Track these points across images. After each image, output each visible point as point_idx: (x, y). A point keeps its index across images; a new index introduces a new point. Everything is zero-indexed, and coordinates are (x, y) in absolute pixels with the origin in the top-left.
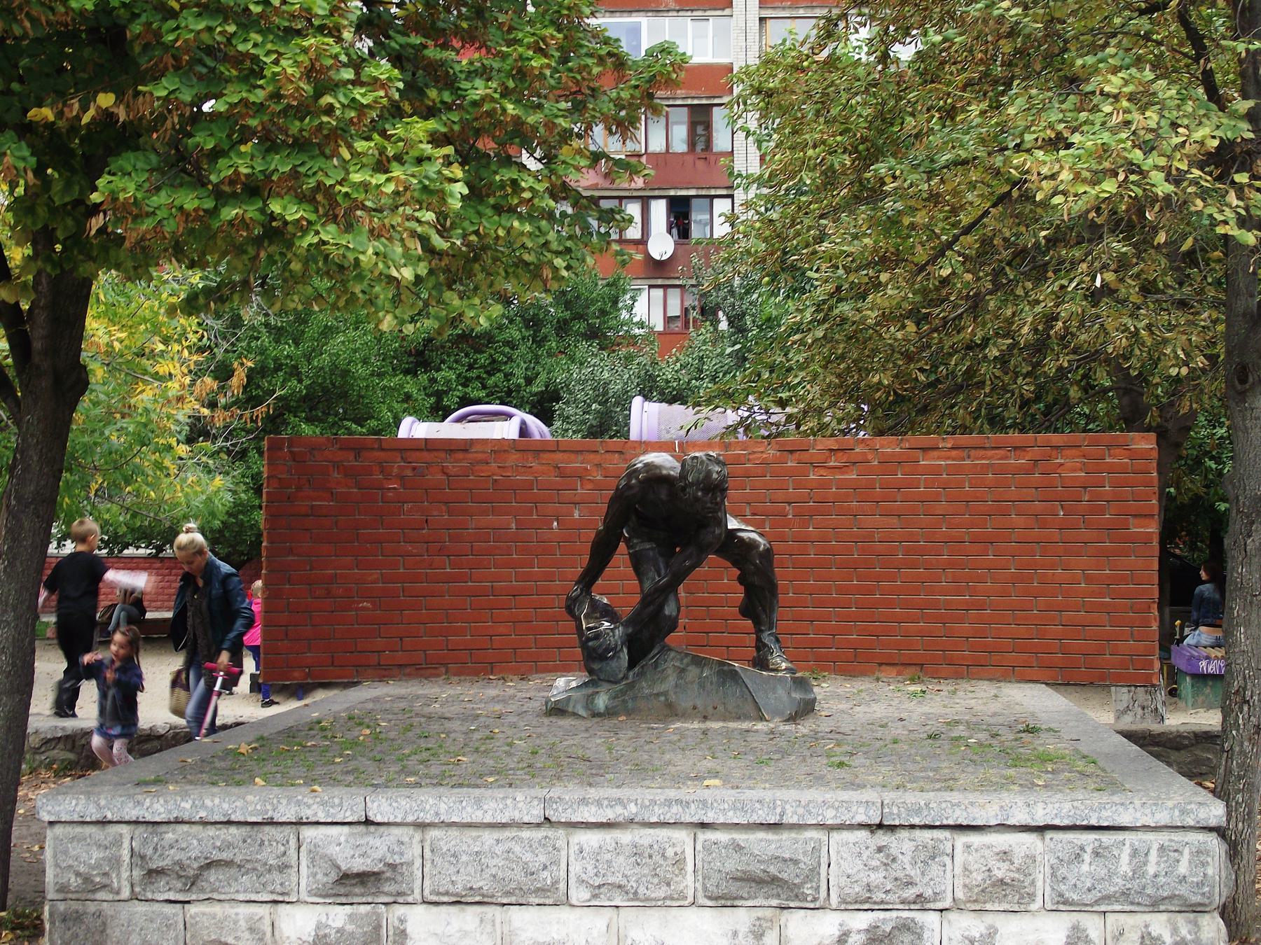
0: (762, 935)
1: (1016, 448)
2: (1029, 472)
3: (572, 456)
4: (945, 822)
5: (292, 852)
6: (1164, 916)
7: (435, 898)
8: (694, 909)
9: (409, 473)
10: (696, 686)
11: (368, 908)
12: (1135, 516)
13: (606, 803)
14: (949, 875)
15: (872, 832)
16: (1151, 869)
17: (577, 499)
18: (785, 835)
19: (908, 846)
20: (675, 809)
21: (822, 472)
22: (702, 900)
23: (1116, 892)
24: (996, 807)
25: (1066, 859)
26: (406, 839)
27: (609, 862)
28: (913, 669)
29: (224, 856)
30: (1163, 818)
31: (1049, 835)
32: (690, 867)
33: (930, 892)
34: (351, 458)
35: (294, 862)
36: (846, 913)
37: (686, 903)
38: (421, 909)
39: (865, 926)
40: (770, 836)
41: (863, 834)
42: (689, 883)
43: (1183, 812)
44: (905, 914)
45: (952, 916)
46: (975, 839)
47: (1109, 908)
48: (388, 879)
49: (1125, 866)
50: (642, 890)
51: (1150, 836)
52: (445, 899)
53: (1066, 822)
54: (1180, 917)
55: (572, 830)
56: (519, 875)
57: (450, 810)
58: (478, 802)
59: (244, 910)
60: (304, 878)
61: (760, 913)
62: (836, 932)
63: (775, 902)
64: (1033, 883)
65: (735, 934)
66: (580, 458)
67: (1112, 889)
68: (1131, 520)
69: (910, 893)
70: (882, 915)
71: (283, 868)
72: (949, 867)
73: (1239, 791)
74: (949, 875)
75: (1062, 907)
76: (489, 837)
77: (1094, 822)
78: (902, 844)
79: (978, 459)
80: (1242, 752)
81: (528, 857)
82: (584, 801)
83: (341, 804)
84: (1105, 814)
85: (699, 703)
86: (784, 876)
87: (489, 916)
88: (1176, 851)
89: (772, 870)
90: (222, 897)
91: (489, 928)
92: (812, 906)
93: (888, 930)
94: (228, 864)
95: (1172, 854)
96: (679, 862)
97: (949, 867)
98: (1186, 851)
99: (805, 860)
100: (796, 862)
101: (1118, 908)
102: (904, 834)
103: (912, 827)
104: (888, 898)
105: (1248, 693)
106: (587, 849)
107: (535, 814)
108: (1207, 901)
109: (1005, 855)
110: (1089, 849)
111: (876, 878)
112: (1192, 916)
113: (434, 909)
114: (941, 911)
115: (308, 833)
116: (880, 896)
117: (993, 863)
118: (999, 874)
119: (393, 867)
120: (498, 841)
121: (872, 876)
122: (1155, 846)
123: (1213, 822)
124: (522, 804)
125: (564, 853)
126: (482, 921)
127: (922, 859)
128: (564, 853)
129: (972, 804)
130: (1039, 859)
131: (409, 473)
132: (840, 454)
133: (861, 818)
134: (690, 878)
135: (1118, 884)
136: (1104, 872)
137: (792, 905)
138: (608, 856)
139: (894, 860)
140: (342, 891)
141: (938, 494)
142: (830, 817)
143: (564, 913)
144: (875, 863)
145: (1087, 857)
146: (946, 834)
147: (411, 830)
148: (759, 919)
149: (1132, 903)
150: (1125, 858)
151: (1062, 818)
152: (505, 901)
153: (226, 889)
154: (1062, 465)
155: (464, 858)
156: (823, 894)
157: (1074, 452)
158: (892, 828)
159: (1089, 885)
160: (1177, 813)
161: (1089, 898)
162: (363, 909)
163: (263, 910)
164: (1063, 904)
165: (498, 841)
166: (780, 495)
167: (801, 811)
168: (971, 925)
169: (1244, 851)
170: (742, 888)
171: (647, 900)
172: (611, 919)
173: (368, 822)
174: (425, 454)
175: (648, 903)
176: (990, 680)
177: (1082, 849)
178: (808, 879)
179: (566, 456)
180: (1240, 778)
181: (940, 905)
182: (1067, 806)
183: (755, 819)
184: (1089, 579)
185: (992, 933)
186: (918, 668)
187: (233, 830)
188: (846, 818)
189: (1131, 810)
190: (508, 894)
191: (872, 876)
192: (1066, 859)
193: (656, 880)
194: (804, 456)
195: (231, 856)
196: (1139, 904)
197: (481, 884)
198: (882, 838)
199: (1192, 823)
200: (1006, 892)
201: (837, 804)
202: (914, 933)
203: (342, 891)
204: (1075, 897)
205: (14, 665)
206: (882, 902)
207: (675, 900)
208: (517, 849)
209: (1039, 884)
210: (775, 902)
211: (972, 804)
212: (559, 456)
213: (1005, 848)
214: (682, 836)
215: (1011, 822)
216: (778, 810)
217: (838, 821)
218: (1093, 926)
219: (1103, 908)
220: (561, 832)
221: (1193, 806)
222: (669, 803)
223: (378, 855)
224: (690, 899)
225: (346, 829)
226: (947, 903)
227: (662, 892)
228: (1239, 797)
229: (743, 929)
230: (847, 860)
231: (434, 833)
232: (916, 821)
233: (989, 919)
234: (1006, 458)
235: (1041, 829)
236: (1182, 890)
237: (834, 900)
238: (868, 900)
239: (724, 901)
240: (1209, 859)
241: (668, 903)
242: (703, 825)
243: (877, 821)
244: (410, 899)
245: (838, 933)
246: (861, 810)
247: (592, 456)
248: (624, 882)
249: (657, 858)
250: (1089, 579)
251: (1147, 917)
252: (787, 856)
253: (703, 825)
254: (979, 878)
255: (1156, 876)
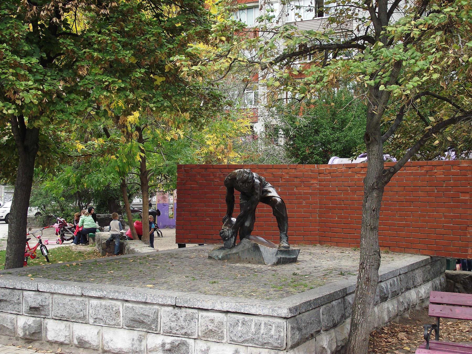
0: (141, 341)
1: (421, 166)
2: (425, 175)
3: (278, 170)
4: (195, 307)
5: (21, 299)
6: (267, 350)
7: (55, 318)
8: (123, 329)
9: (222, 176)
10: (247, 251)
11: (39, 319)
12: (462, 192)
13: (98, 290)
14: (197, 326)
15: (174, 308)
16: (262, 331)
17: (279, 185)
18: (148, 306)
19: (184, 314)
20: (117, 294)
21: (359, 175)
22: (125, 327)
23: (249, 339)
24: (211, 303)
25: (233, 324)
26: (47, 297)
27: (98, 310)
28: (387, 248)
29: (4, 298)
30: (266, 312)
31: (229, 314)
32: (121, 315)
33: (190, 332)
34: (204, 171)
35: (22, 302)
36: (166, 336)
37: (120, 327)
38: (52, 320)
39: (170, 342)
40: (144, 306)
41: (171, 308)
42: (121, 320)
43: (273, 310)
44: (184, 339)
45: (198, 341)
46: (205, 314)
47: (248, 345)
48: (42, 310)
49: (253, 329)
50: (107, 321)
51: (262, 319)
52: (57, 318)
53: (233, 310)
54: (272, 351)
55: (90, 299)
56: (74, 312)
57: (58, 289)
58: (65, 288)
59: (10, 316)
60: (24, 308)
61: (141, 333)
62: (161, 343)
63: (145, 330)
64: (222, 332)
65: (133, 340)
66: (281, 170)
67: (248, 338)
68: (460, 194)
69: (183, 331)
70: (176, 338)
71: (19, 303)
72: (197, 323)
73: (359, 304)
74: (197, 326)
75: (232, 343)
76: (68, 298)
77: (242, 311)
78: (182, 313)
79: (408, 170)
80: (362, 288)
81: (77, 306)
82: (92, 289)
83: (31, 285)
84: (246, 308)
85: (248, 257)
86: (145, 321)
87: (68, 325)
88: (270, 325)
89: (142, 318)
90: (5, 311)
91: (68, 329)
92: (155, 332)
93: (177, 344)
94: (6, 301)
95: (269, 326)
96: (117, 312)
97: (197, 323)
98: (274, 326)
99: (152, 316)
100: (149, 316)
101: (251, 345)
102: (183, 310)
103: (186, 307)
104: (178, 332)
105: (365, 265)
106: (93, 306)
107: (78, 292)
108: (280, 346)
109: (212, 321)
110: (240, 321)
111: (173, 325)
112: (276, 351)
113: (55, 321)
114: (195, 339)
115: (25, 293)
116: (174, 331)
117: (209, 323)
118: (210, 328)
119: (43, 306)
120: (70, 300)
121: (172, 324)
122: (263, 323)
123: (283, 315)
124: (75, 288)
125: (88, 306)
126: (66, 326)
127: (189, 319)
128: (88, 306)
129: (203, 300)
130: (224, 323)
131: (222, 176)
132: (364, 169)
133: (169, 303)
134: (121, 318)
135: (250, 336)
136: (245, 331)
137: (150, 331)
138: (98, 309)
139: (179, 319)
140: (32, 312)
141: (396, 183)
142: (160, 301)
143: (87, 327)
144: (173, 319)
145: (240, 324)
146: (196, 311)
147: (49, 294)
148: (140, 335)
149: (255, 344)
150: (253, 326)
151: (232, 309)
152: (73, 321)
153: (6, 309)
154: (436, 172)
155: (61, 305)
156: (159, 329)
157: (441, 167)
158: (180, 307)
159: (240, 335)
160: (271, 310)
161: (240, 340)
162: (38, 319)
163: (14, 316)
164: (232, 342)
165: (70, 300)
166: (346, 184)
167: (152, 298)
168: (201, 345)
169: (360, 328)
170: (135, 323)
171: (109, 325)
172: (100, 330)
173: (38, 291)
174: (227, 170)
175: (110, 326)
176: (411, 254)
177: (238, 321)
178: (152, 323)
179: (275, 170)
180: (360, 298)
181: (194, 337)
182: (234, 304)
183: (138, 300)
184: (445, 217)
185: (208, 349)
186: (388, 248)
187: (8, 290)
188: (164, 302)
189: (255, 308)
190: (73, 318)
191: (172, 324)
192: (233, 324)
193: (111, 318)
194: (354, 170)
195: (6, 298)
196: (257, 344)
197: (65, 314)
198: (177, 310)
199: (276, 315)
200: (211, 335)
201: (162, 297)
202: (186, 346)
203: (32, 312)
204: (236, 339)
205: (16, 235)
206: (175, 334)
207: (116, 326)
208: (75, 303)
209: (225, 333)
210: (145, 330)
211: (203, 300)
212: (273, 170)
213: (212, 318)
214: (119, 303)
215: (216, 308)
216: (145, 297)
217: (162, 303)
218: (242, 350)
219: (246, 344)
220: (87, 299)
221: (276, 308)
222: (115, 292)
223: (38, 302)
224: (121, 326)
225: (34, 293)
226: (196, 337)
227: (112, 323)
228: (359, 306)
229: (136, 338)
230: (165, 316)
231: (55, 296)
232: (186, 305)
233: (209, 344)
234: (418, 170)
235: (227, 312)
236: (271, 341)
237: (162, 332)
238: (171, 332)
239: (130, 327)
240: (282, 330)
241: (115, 326)
242: (127, 301)
243: (174, 304)
244: (49, 317)
245: (161, 343)
246: (170, 300)
247: (285, 170)
248: (102, 318)
249: (111, 310)
250: (445, 217)
251: (261, 350)
252: (146, 314)
253: (127, 301)
254: (204, 328)
255: (263, 334)
